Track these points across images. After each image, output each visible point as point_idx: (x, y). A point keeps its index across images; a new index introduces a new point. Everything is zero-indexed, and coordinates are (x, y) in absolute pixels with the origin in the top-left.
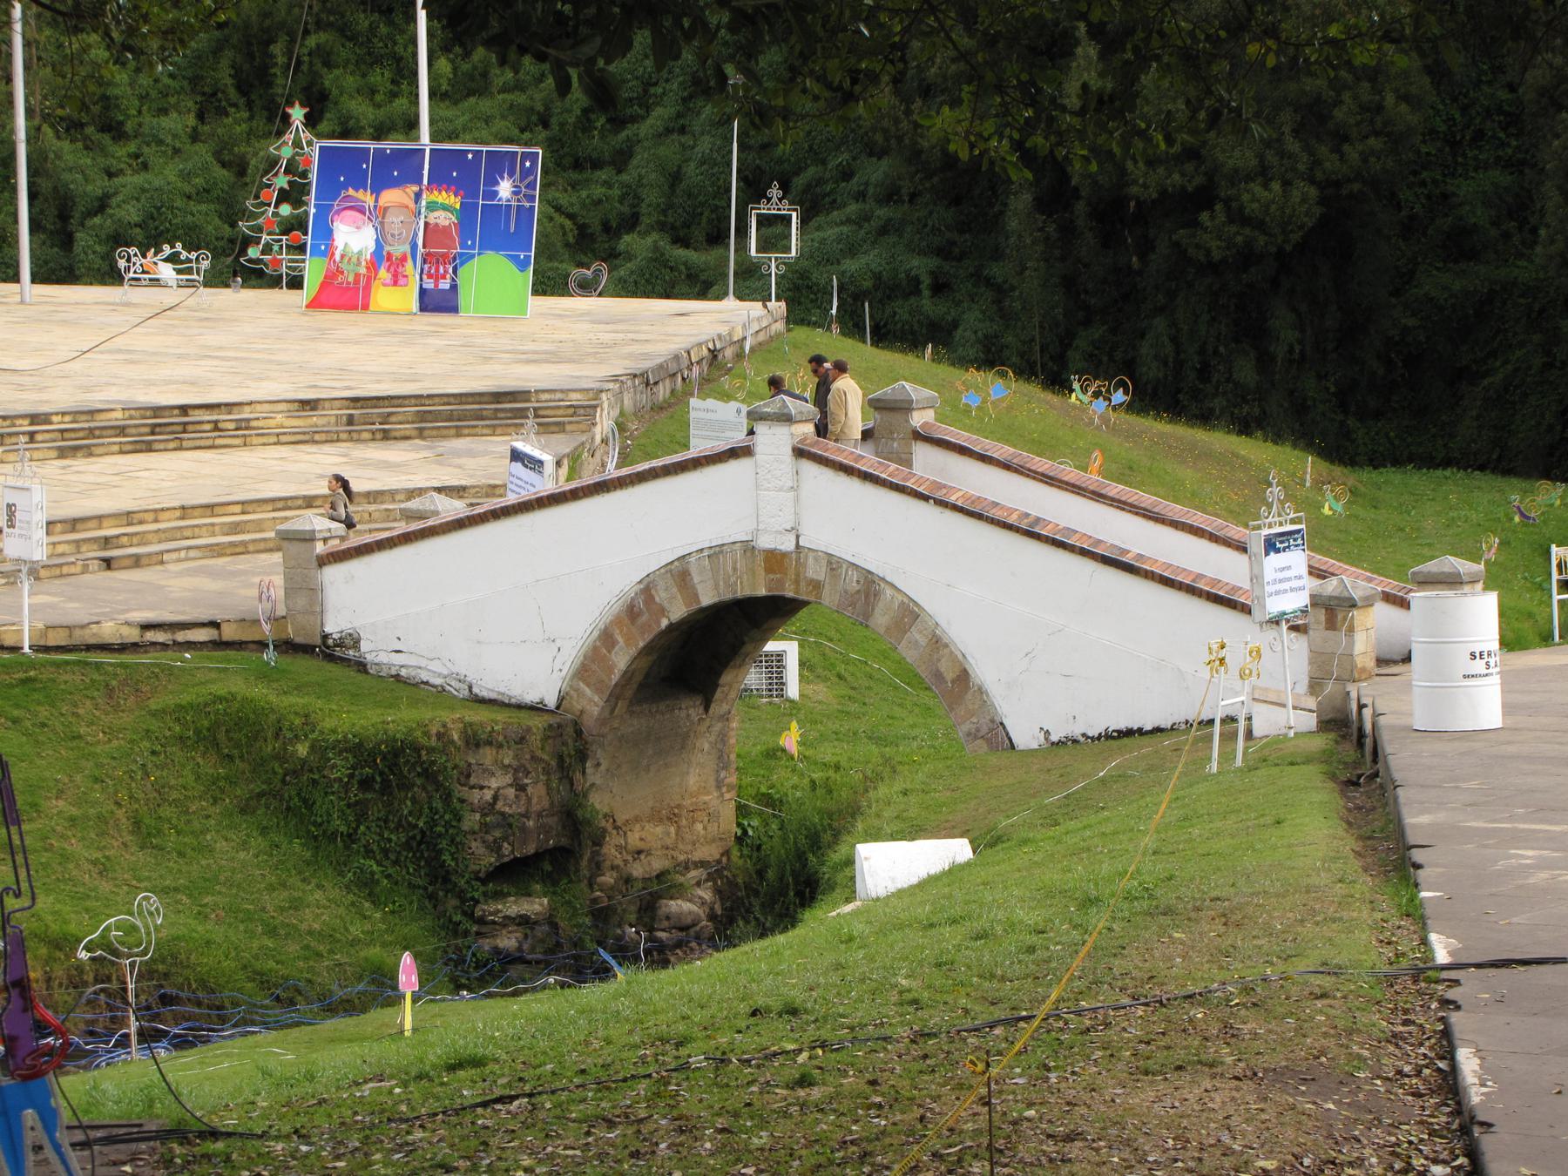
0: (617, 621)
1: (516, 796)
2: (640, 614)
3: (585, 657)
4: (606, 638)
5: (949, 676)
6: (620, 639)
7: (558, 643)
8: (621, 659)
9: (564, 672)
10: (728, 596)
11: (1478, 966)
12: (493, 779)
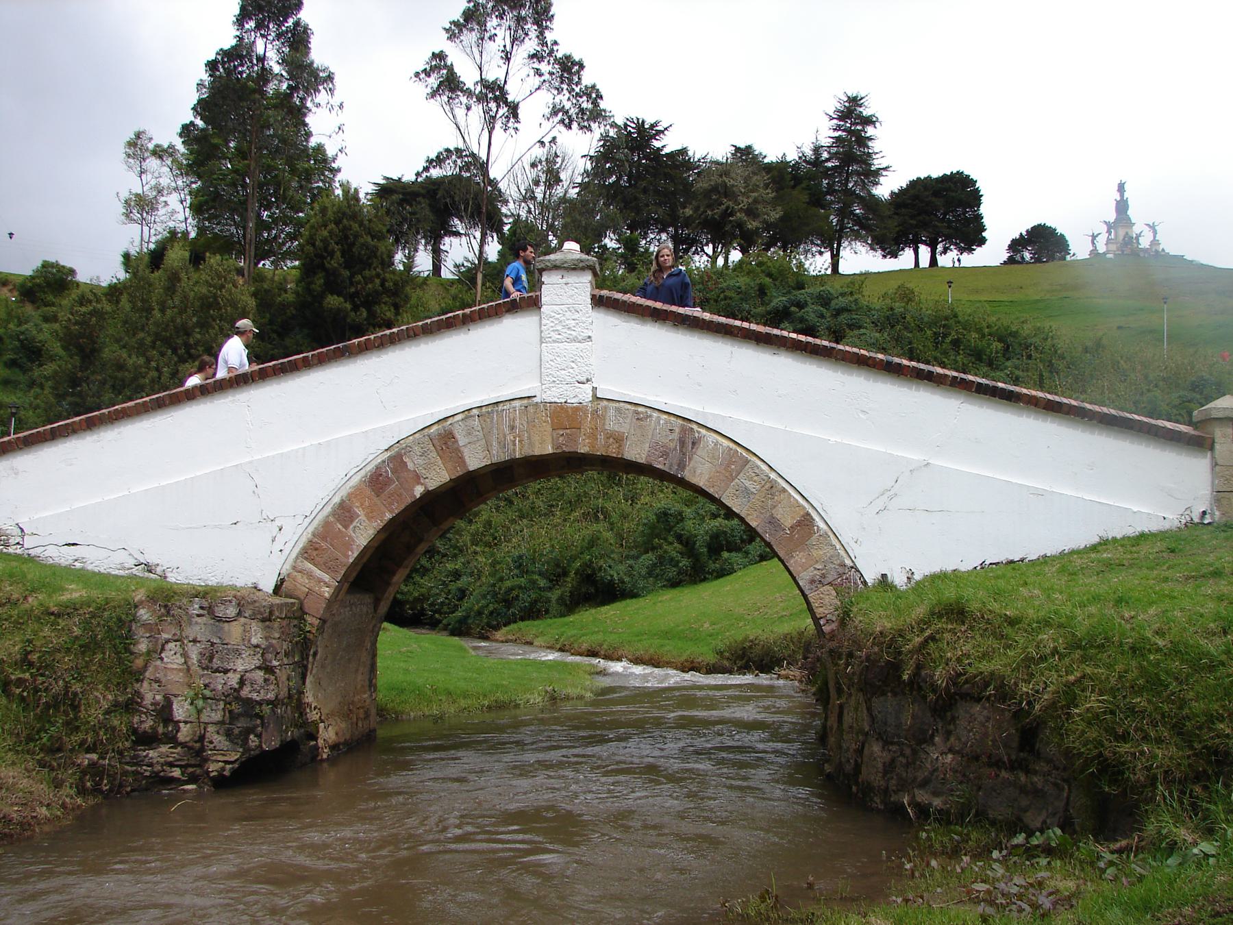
0: (355, 494)
1: (266, 680)
2: (388, 482)
3: (314, 535)
4: (344, 512)
5: (788, 522)
6: (360, 511)
7: (278, 523)
8: (363, 534)
9: (286, 552)
10: (502, 457)
11: (460, 130)
12: (240, 661)
